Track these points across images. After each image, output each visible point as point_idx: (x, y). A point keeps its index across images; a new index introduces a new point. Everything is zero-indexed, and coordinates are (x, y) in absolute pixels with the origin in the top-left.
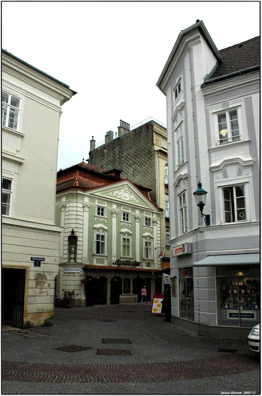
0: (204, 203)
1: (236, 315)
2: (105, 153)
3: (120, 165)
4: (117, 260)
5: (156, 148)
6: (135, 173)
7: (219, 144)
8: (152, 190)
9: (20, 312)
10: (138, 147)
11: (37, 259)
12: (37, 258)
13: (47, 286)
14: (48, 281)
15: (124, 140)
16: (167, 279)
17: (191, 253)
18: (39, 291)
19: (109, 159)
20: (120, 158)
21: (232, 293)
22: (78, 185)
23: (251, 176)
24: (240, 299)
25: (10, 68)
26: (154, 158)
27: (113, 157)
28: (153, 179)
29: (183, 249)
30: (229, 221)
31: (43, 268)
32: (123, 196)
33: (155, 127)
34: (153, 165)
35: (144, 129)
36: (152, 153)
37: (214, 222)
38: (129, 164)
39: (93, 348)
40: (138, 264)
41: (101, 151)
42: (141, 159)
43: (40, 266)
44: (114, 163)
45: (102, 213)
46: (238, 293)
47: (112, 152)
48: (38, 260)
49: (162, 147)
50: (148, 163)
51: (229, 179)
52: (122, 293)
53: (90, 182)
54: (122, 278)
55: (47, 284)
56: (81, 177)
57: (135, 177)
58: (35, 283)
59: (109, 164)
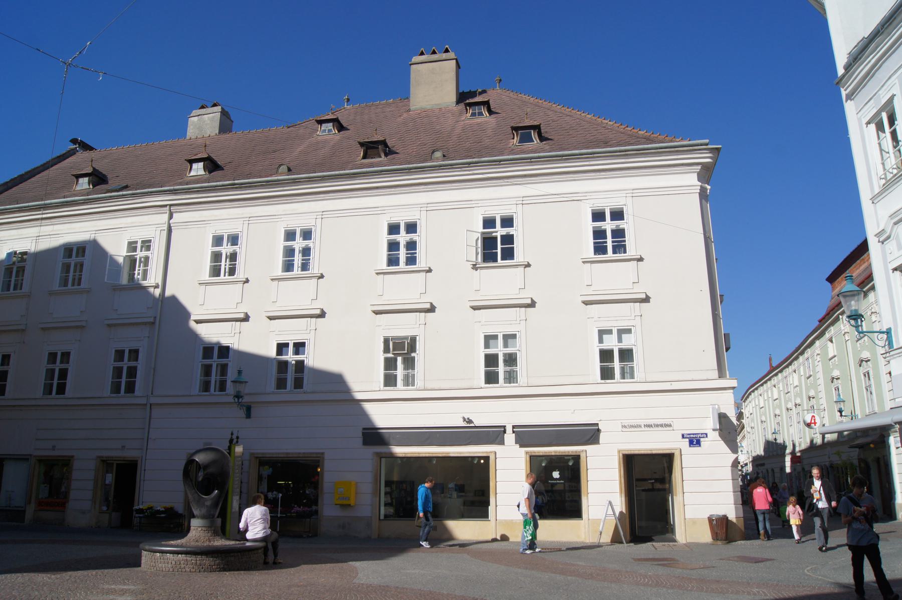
7: (417, 337)
11: (692, 436)
12: (693, 434)
25: (377, 188)
30: (408, 385)
39: (716, 567)
43: (700, 446)
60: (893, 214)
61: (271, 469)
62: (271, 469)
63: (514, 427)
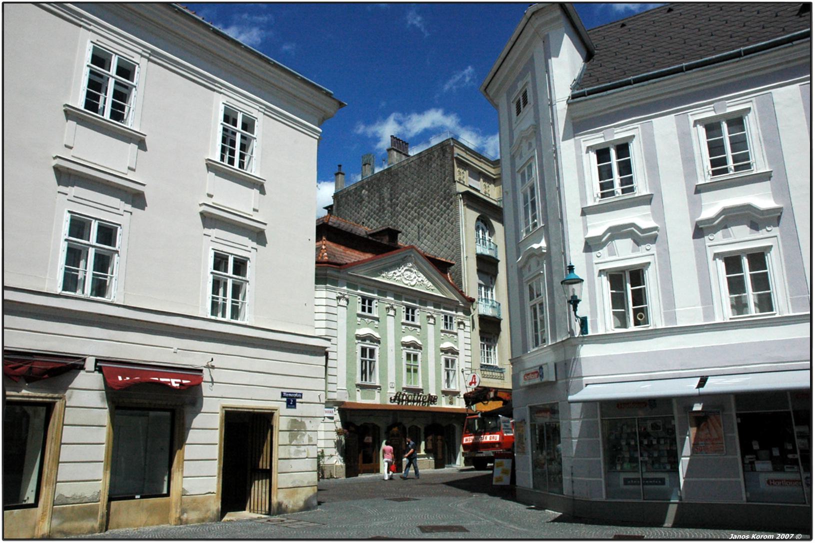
0: (578, 298)
1: (635, 482)
2: (364, 196)
3: (392, 218)
4: (397, 393)
5: (460, 188)
6: (420, 233)
8: (453, 265)
9: (264, 487)
10: (426, 186)
11: (290, 395)
12: (291, 393)
13: (307, 441)
14: (308, 433)
15: (400, 173)
16: (507, 424)
17: (554, 380)
19: (372, 207)
20: (393, 205)
21: (626, 444)
22: (327, 258)
23: (655, 252)
24: (641, 455)
26: (457, 206)
27: (380, 205)
28: (454, 244)
29: (541, 374)
31: (300, 409)
32: (406, 277)
33: (457, 151)
34: (455, 218)
35: (436, 154)
36: (451, 197)
37: (595, 327)
38: (409, 216)
40: (433, 399)
41: (355, 193)
42: (432, 209)
43: (295, 407)
44: (381, 215)
45: (369, 308)
46: (637, 446)
47: (376, 195)
48: (293, 397)
49: (470, 187)
50: (445, 215)
51: (618, 258)
53: (347, 252)
54: (406, 425)
56: (331, 244)
57: (421, 240)
59: (371, 217)
63: (97, 361)
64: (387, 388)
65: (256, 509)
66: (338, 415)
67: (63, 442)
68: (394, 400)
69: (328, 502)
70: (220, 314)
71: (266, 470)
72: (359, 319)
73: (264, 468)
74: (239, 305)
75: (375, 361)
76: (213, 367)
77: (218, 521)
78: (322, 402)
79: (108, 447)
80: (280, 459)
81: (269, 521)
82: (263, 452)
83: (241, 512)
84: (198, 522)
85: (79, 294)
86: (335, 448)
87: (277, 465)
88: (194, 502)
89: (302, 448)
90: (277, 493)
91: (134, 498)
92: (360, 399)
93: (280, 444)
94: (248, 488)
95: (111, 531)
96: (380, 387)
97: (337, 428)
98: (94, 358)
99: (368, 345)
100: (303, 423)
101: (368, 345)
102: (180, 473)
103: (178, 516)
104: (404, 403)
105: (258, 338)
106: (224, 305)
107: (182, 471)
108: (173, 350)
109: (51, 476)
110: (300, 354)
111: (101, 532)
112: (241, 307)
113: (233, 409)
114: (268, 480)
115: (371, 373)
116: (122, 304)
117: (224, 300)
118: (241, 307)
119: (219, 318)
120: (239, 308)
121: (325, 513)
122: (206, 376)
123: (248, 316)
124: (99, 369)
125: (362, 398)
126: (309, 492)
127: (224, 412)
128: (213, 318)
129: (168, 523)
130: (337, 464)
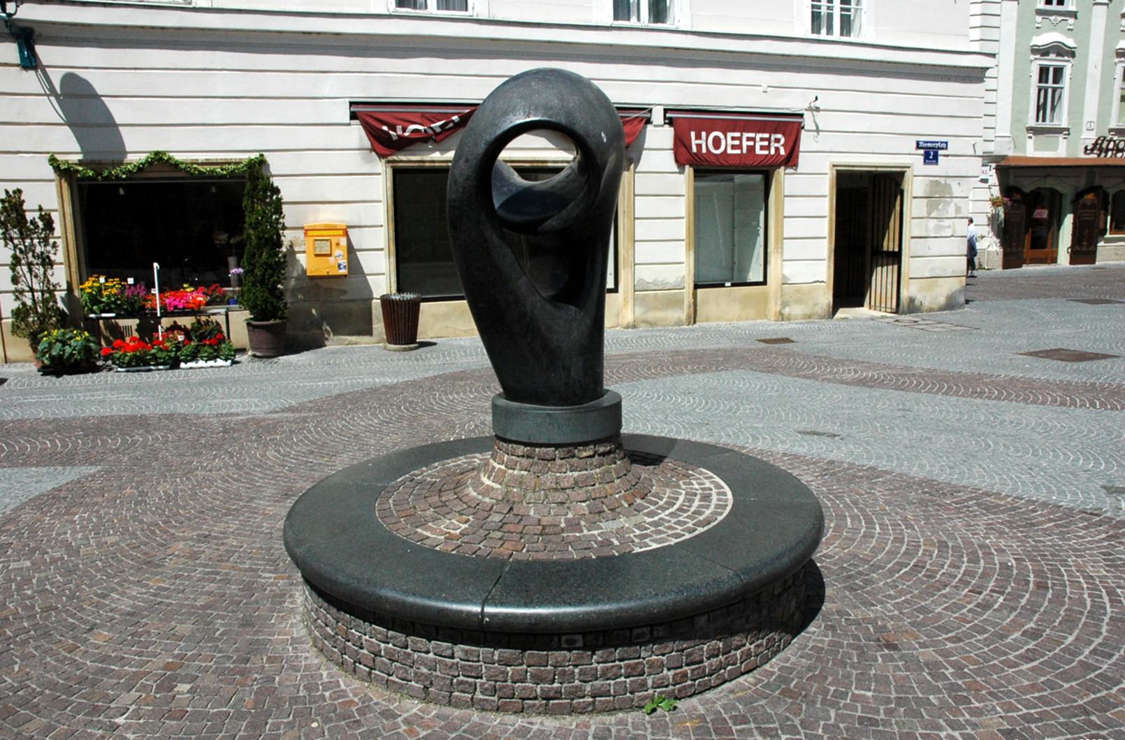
4: (1099, 139)
9: (890, 276)
11: (929, 145)
12: (931, 142)
13: (954, 212)
18: (936, 225)
31: (945, 165)
43: (937, 163)
48: (933, 148)
52: (1105, 234)
55: (954, 208)
58: (925, 205)
60: (62, 193)
61: (687, 167)
62: (687, 167)
63: (666, 111)
64: (1080, 132)
65: (878, 304)
66: (995, 176)
67: (636, 216)
68: (1092, 150)
69: (980, 300)
70: (824, 31)
71: (893, 252)
72: (1039, 18)
73: (891, 249)
74: (852, 13)
75: (1062, 88)
76: (817, 109)
77: (829, 318)
78: (977, 154)
79: (689, 222)
80: (913, 238)
81: (897, 321)
82: (888, 228)
83: (857, 309)
84: (804, 318)
85: (633, 22)
86: (988, 225)
87: (909, 247)
88: (798, 293)
89: (946, 222)
90: (908, 284)
91: (723, 285)
92: (1033, 151)
93: (914, 216)
94: (867, 277)
95: (700, 324)
96: (1068, 129)
97: (992, 195)
98: (662, 108)
99: (1052, 61)
100: (948, 186)
101: (1052, 61)
102: (779, 255)
103: (778, 309)
104: (1110, 154)
105: (881, 62)
106: (830, 17)
107: (782, 252)
108: (761, 89)
109: (628, 256)
110: (945, 81)
111: (689, 324)
112: (855, 17)
113: (846, 168)
114: (896, 267)
115: (1053, 108)
116: (690, 29)
117: (829, 8)
118: (855, 17)
119: (823, 35)
120: (852, 18)
121: (975, 314)
122: (808, 122)
123: (866, 30)
124: (671, 122)
125: (1036, 149)
126: (956, 284)
127: (835, 172)
128: (815, 36)
129: (766, 317)
130: (990, 249)
